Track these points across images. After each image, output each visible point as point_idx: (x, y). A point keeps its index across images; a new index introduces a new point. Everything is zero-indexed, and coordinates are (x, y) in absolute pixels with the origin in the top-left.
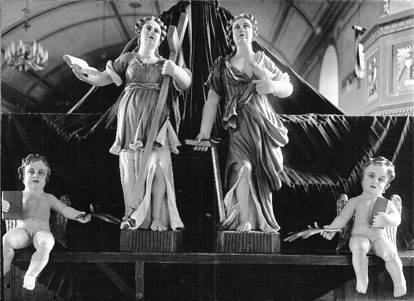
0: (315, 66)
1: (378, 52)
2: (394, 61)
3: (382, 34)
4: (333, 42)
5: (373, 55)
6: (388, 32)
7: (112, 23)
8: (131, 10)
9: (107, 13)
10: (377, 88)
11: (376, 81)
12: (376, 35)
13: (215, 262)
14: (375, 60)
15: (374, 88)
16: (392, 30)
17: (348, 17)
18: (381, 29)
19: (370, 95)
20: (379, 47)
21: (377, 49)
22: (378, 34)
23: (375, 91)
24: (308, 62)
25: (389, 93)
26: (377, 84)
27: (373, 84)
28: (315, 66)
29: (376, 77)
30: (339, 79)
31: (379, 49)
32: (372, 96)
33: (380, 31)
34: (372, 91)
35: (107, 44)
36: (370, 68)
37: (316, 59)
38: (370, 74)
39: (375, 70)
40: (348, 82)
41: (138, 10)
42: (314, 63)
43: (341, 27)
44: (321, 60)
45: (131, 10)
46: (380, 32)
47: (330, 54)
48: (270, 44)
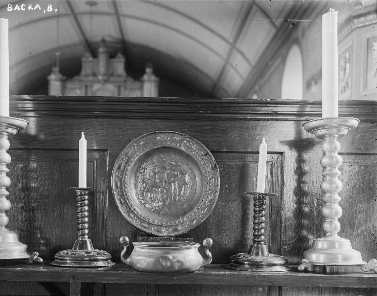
0: (279, 66)
1: (351, 46)
2: (369, 56)
3: (356, 26)
4: (297, 42)
5: (346, 50)
6: (363, 25)
7: (67, 24)
8: (87, 8)
9: (62, 11)
10: (349, 85)
11: (349, 77)
12: (349, 27)
13: (100, 264)
14: (347, 55)
15: (346, 85)
16: (368, 21)
17: (267, 75)
18: (356, 21)
19: (341, 93)
20: (352, 40)
21: (350, 43)
22: (351, 27)
23: (347, 88)
24: (270, 63)
25: (364, 91)
26: (349, 81)
27: (345, 81)
28: (279, 66)
29: (349, 73)
30: (303, 78)
31: (353, 42)
32: (343, 93)
33: (354, 23)
34: (344, 89)
35: (62, 43)
36: (342, 63)
37: (279, 60)
38: (342, 70)
39: (348, 65)
40: (313, 83)
41: (95, 9)
42: (276, 64)
43: (307, 25)
44: (284, 60)
45: (87, 8)
46: (354, 25)
47: (294, 56)
48: (231, 44)
